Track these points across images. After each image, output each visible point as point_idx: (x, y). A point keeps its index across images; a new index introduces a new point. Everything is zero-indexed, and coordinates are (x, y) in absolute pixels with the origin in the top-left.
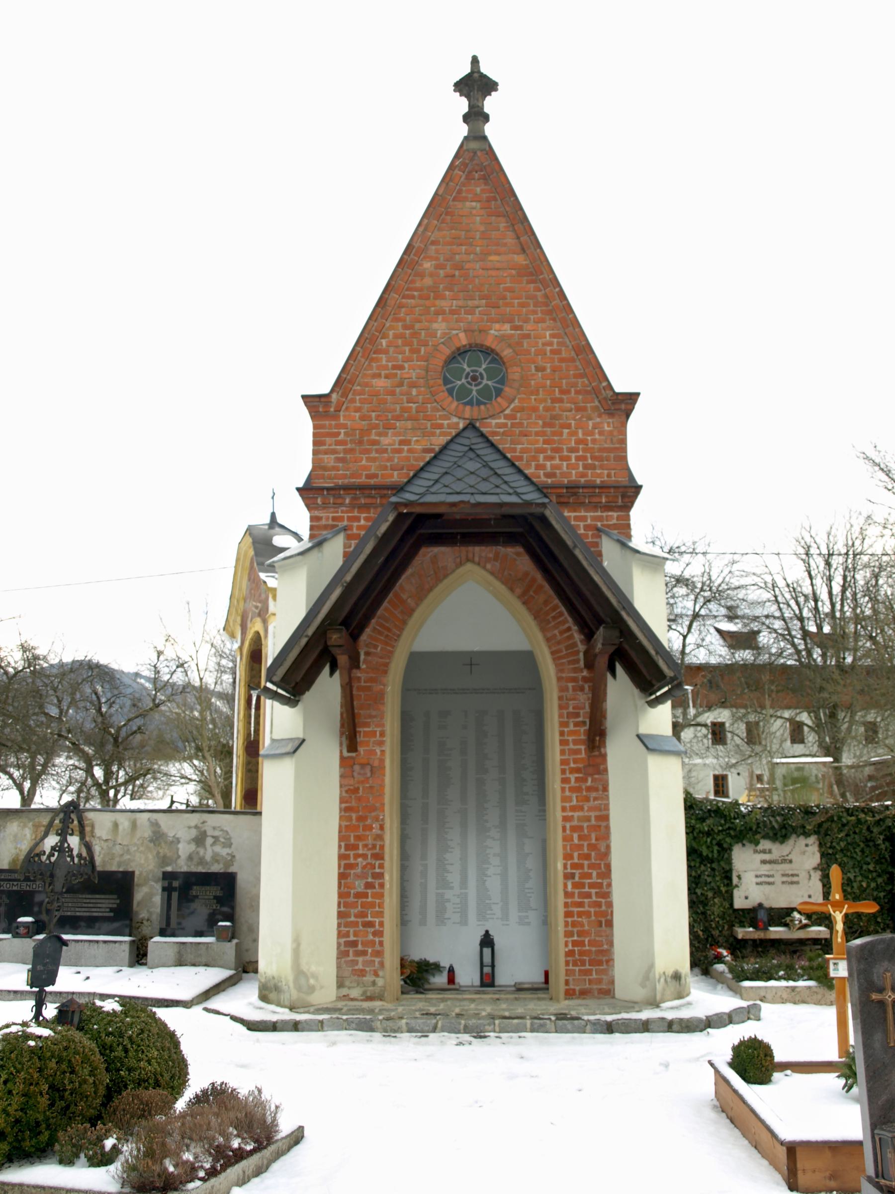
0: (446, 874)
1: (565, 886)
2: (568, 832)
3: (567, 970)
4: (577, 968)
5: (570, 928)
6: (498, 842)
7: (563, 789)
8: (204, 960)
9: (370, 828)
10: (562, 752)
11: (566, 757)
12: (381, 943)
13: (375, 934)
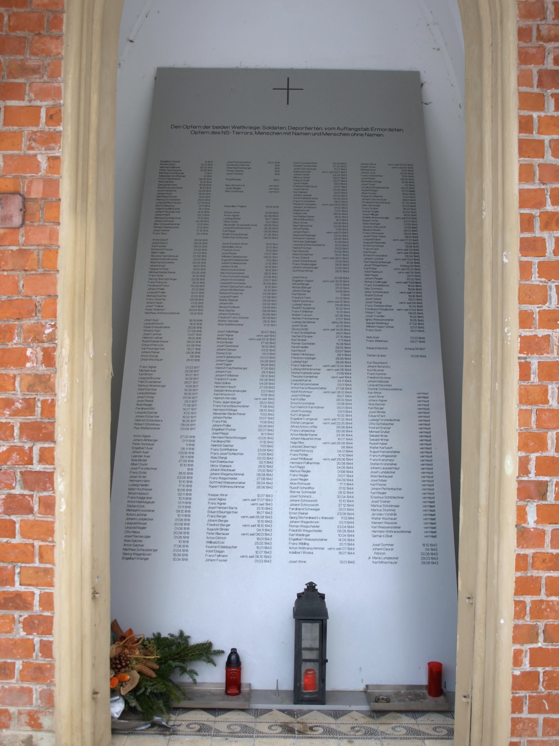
0: (230, 458)
1: (521, 514)
2: (534, 379)
3: (515, 722)
4: (541, 717)
5: (528, 620)
6: (335, 396)
7: (525, 269)
9: (20, 359)
10: (526, 173)
11: (536, 186)
12: (47, 649)
13: (30, 625)
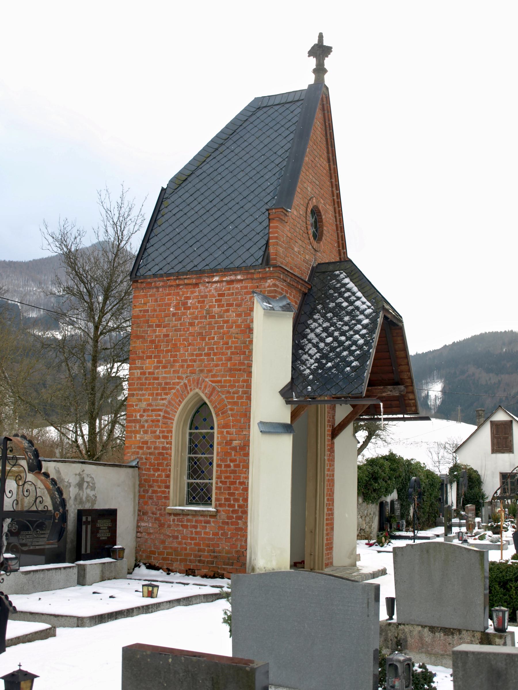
8: (113, 575)
